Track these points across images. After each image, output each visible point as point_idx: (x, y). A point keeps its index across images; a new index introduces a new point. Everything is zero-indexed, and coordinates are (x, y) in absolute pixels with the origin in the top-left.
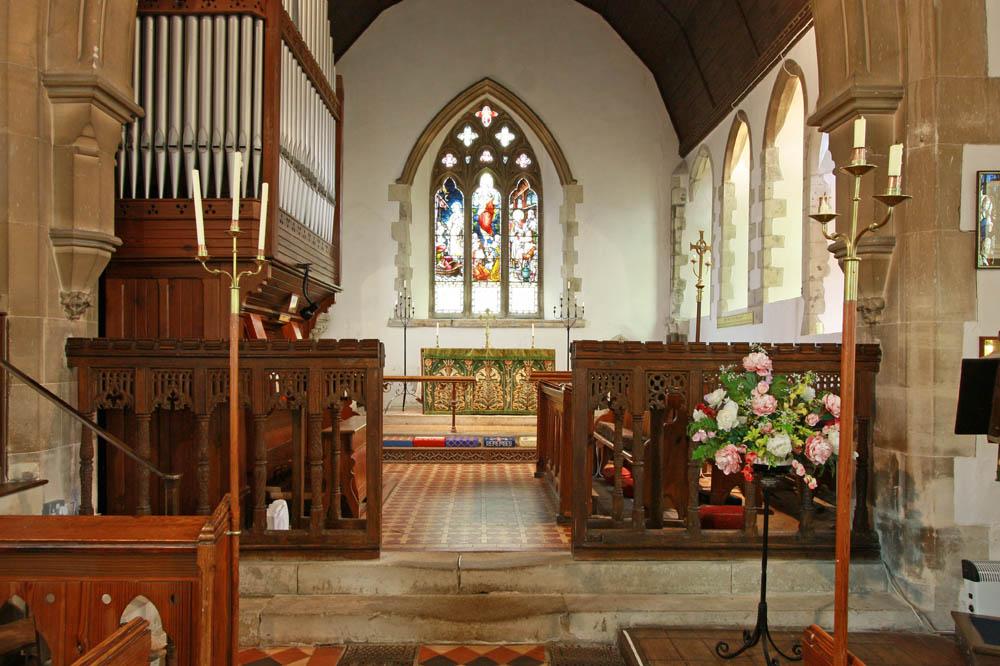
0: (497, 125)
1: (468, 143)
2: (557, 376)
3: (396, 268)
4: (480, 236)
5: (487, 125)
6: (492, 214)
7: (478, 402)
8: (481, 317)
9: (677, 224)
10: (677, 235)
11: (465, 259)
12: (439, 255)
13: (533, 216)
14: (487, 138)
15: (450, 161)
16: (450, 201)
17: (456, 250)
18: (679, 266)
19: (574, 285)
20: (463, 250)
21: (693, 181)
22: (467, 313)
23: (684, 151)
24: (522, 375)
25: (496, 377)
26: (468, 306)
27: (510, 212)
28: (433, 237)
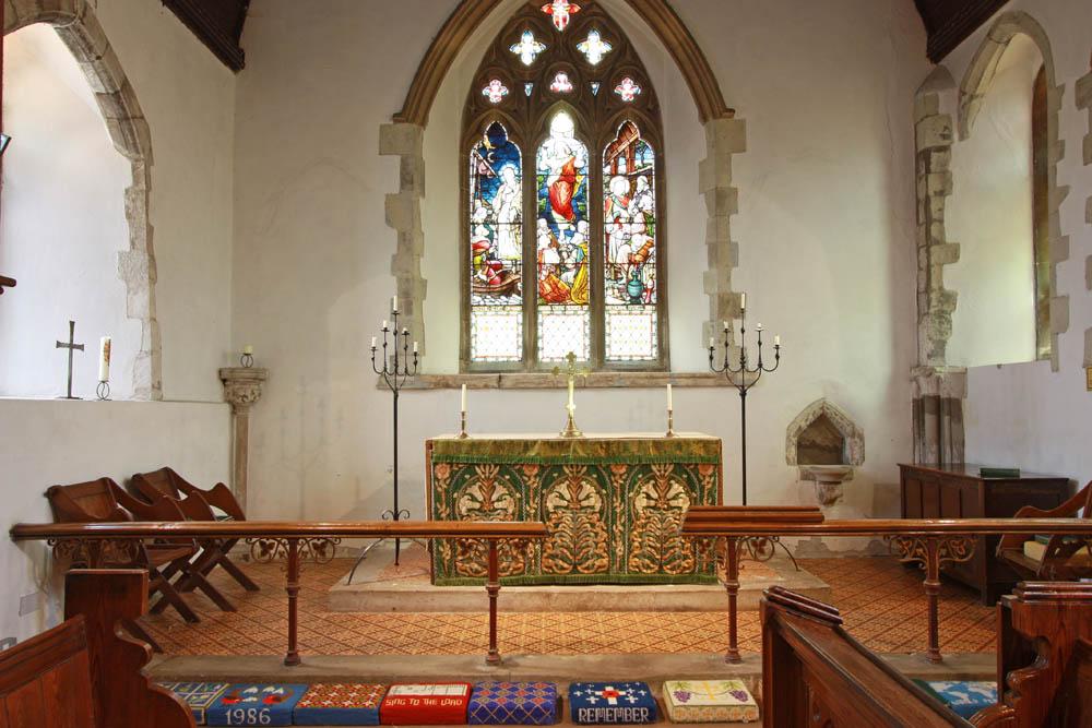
0: (578, 29)
1: (527, 60)
2: (753, 520)
3: (395, 278)
4: (552, 223)
5: (561, 28)
6: (572, 184)
7: (553, 557)
8: (556, 371)
9: (934, 184)
10: (934, 206)
11: (525, 264)
12: (478, 259)
13: (647, 187)
14: (562, 51)
15: (495, 91)
16: (497, 162)
17: (508, 248)
18: (941, 265)
19: (728, 307)
20: (520, 248)
21: (966, 98)
22: (530, 362)
23: (937, 52)
24: (649, 497)
25: (592, 501)
26: (530, 348)
27: (606, 179)
28: (466, 226)
